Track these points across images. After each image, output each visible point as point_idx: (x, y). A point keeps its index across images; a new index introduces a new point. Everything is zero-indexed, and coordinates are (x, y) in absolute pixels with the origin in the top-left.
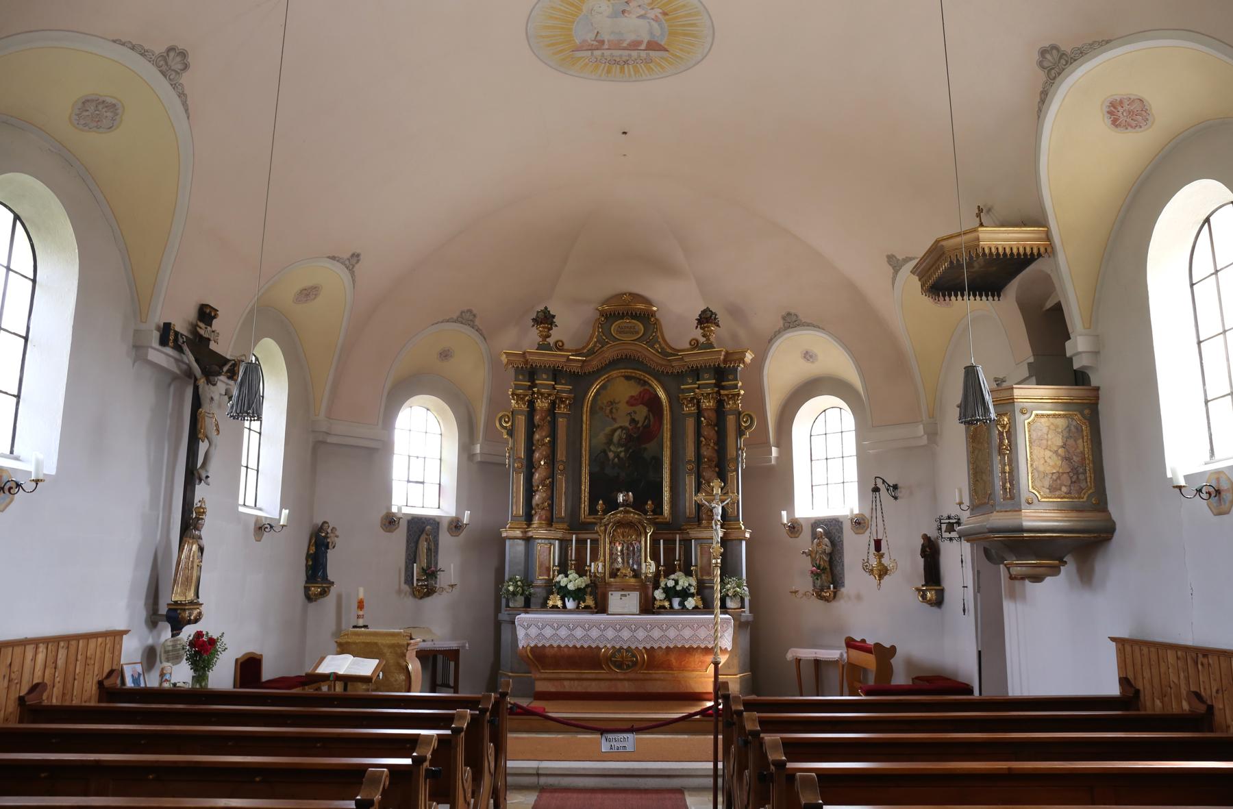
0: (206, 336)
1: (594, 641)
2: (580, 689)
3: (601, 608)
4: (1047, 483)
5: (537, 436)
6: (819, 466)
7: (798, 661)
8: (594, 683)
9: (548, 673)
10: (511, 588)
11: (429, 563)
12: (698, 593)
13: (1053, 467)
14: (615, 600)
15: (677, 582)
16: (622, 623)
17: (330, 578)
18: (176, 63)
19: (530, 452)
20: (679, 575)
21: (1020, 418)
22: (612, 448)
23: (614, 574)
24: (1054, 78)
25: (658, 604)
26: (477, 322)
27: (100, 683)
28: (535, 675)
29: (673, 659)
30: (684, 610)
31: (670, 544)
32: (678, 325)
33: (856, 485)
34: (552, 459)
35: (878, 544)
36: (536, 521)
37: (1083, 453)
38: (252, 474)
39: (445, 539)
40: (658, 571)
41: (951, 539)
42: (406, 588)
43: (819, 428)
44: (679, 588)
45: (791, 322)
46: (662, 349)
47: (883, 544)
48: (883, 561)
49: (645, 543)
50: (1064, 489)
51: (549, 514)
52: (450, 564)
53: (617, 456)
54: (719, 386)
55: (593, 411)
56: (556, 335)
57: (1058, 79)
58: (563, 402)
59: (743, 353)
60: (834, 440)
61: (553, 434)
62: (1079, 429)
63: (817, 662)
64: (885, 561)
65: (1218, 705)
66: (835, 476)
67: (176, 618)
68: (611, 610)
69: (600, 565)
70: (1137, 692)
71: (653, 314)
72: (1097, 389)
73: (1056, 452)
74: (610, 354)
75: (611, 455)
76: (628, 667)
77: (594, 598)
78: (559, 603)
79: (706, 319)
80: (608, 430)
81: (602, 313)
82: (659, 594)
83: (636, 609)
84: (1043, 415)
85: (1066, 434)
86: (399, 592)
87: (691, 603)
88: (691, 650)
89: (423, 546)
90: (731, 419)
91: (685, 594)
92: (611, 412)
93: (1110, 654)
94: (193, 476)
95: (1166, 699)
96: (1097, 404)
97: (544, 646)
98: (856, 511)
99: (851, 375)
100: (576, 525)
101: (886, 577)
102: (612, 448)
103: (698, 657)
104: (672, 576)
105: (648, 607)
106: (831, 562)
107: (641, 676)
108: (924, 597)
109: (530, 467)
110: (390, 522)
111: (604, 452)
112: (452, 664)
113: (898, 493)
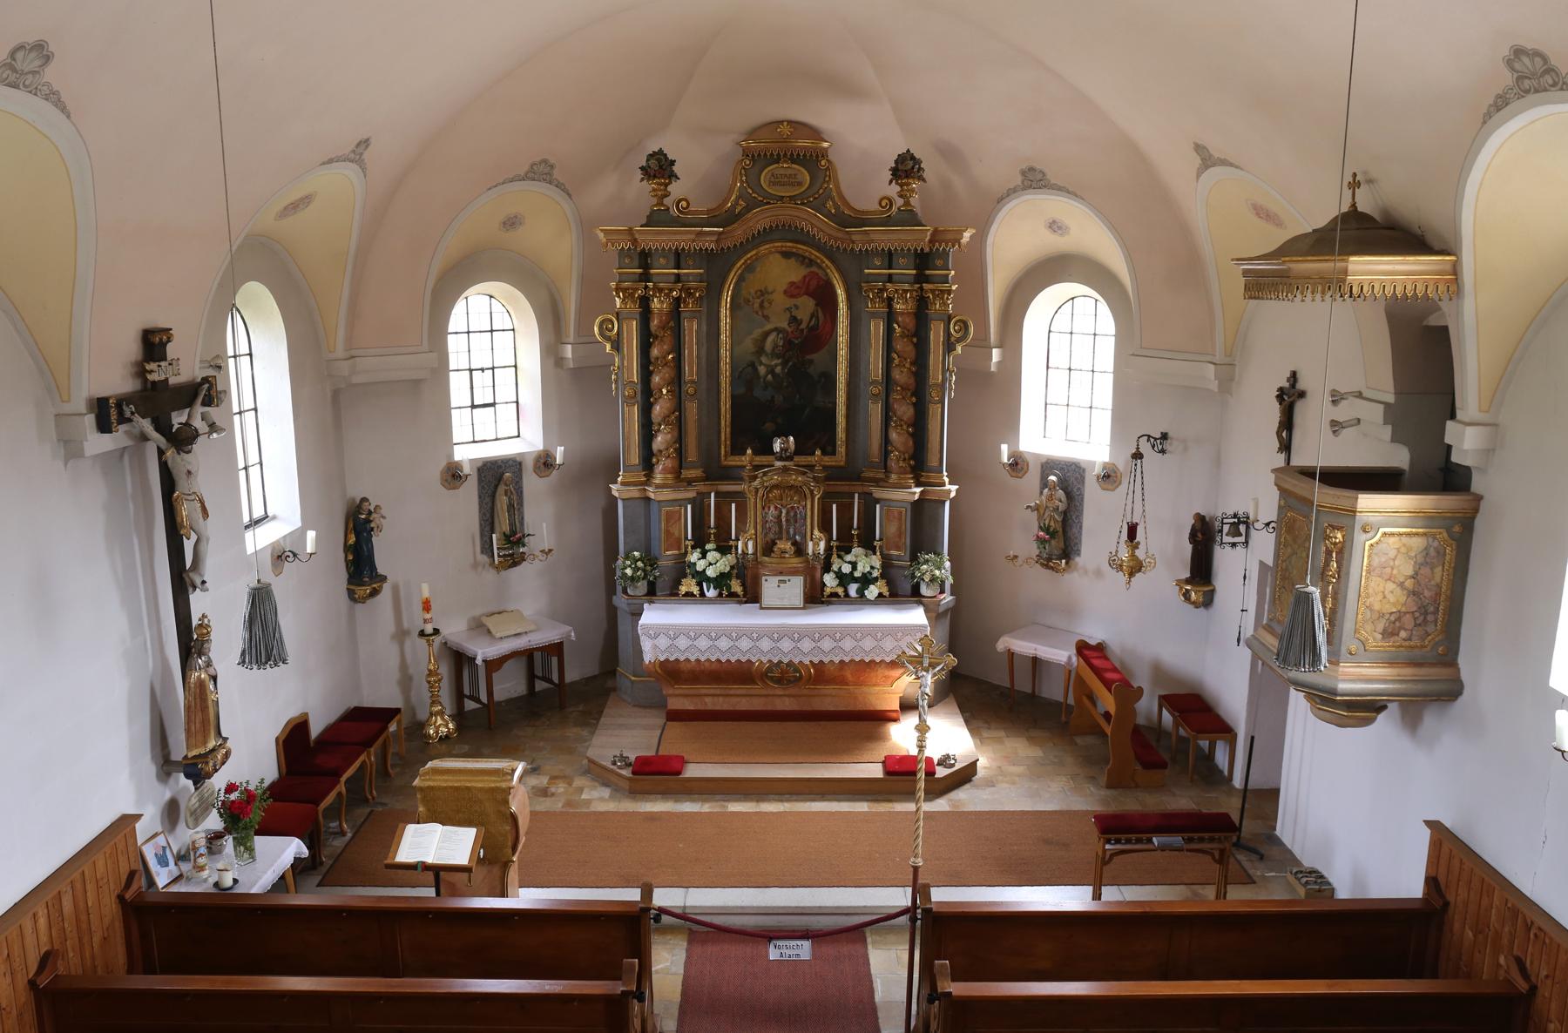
0: (163, 377)
1: (744, 653)
2: (726, 707)
3: (752, 596)
4: (1381, 626)
5: (655, 352)
6: (1059, 378)
7: (1011, 654)
8: (744, 700)
9: (685, 688)
10: (629, 572)
11: (512, 524)
12: (883, 576)
13: (1394, 604)
14: (771, 588)
15: (854, 565)
16: (777, 624)
17: (381, 571)
18: (27, 62)
19: (646, 375)
20: (857, 551)
21: (1359, 537)
22: (764, 359)
23: (768, 549)
24: (1527, 92)
25: (828, 591)
26: (556, 174)
27: (121, 898)
28: (667, 691)
29: (848, 674)
30: (861, 600)
31: (845, 512)
32: (865, 183)
33: (1109, 413)
34: (677, 380)
35: (1132, 530)
36: (658, 478)
37: (1439, 586)
38: (254, 472)
39: (533, 485)
40: (829, 549)
41: (1234, 545)
42: (485, 559)
43: (1062, 322)
44: (857, 574)
45: (1034, 180)
46: (837, 207)
47: (1140, 531)
48: (1137, 552)
49: (811, 510)
50: (1403, 634)
51: (676, 464)
52: (542, 517)
53: (771, 371)
54: (921, 278)
55: (734, 307)
56: (676, 189)
57: (1531, 97)
58: (690, 295)
59: (960, 233)
60: (1082, 344)
61: (678, 349)
62: (1441, 554)
63: (1035, 661)
64: (1140, 553)
65: (1544, 991)
66: (1080, 396)
67: (197, 771)
68: (766, 601)
69: (750, 544)
70: (1447, 904)
71: (824, 154)
72: (1479, 498)
73: (1401, 585)
74: (759, 220)
75: (762, 370)
76: (789, 682)
77: (743, 587)
78: (695, 590)
79: (906, 168)
80: (757, 333)
81: (746, 153)
82: (830, 580)
83: (798, 600)
84: (1392, 534)
85: (1420, 559)
86: (475, 565)
87: (872, 592)
88: (872, 664)
89: (502, 501)
90: (936, 334)
91: (866, 581)
92: (761, 305)
93: (1422, 840)
94: (182, 583)
95: (1481, 937)
96: (1473, 518)
97: (677, 660)
98: (1107, 459)
99: (1117, 263)
100: (716, 473)
101: (1138, 575)
102: (764, 359)
103: (882, 672)
104: (849, 558)
105: (815, 597)
106: (1064, 522)
107: (805, 692)
108: (1186, 595)
109: (647, 396)
110: (453, 475)
111: (753, 365)
112: (555, 660)
113: (1167, 446)
